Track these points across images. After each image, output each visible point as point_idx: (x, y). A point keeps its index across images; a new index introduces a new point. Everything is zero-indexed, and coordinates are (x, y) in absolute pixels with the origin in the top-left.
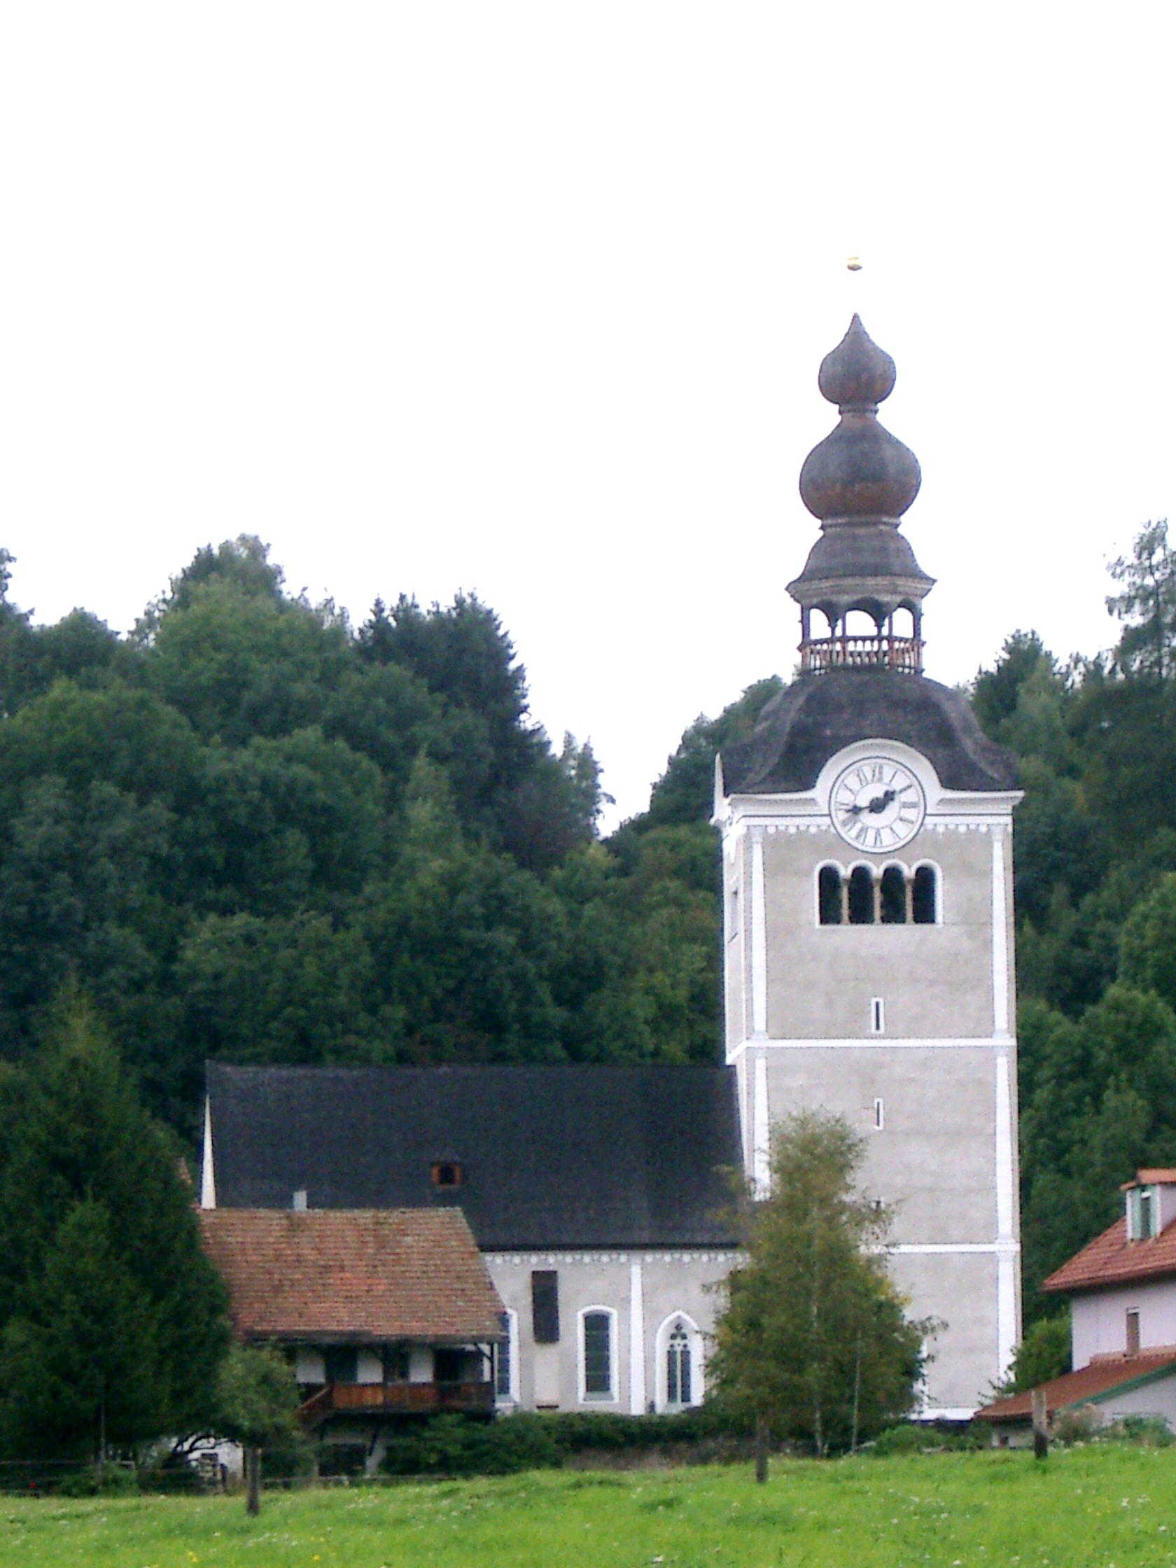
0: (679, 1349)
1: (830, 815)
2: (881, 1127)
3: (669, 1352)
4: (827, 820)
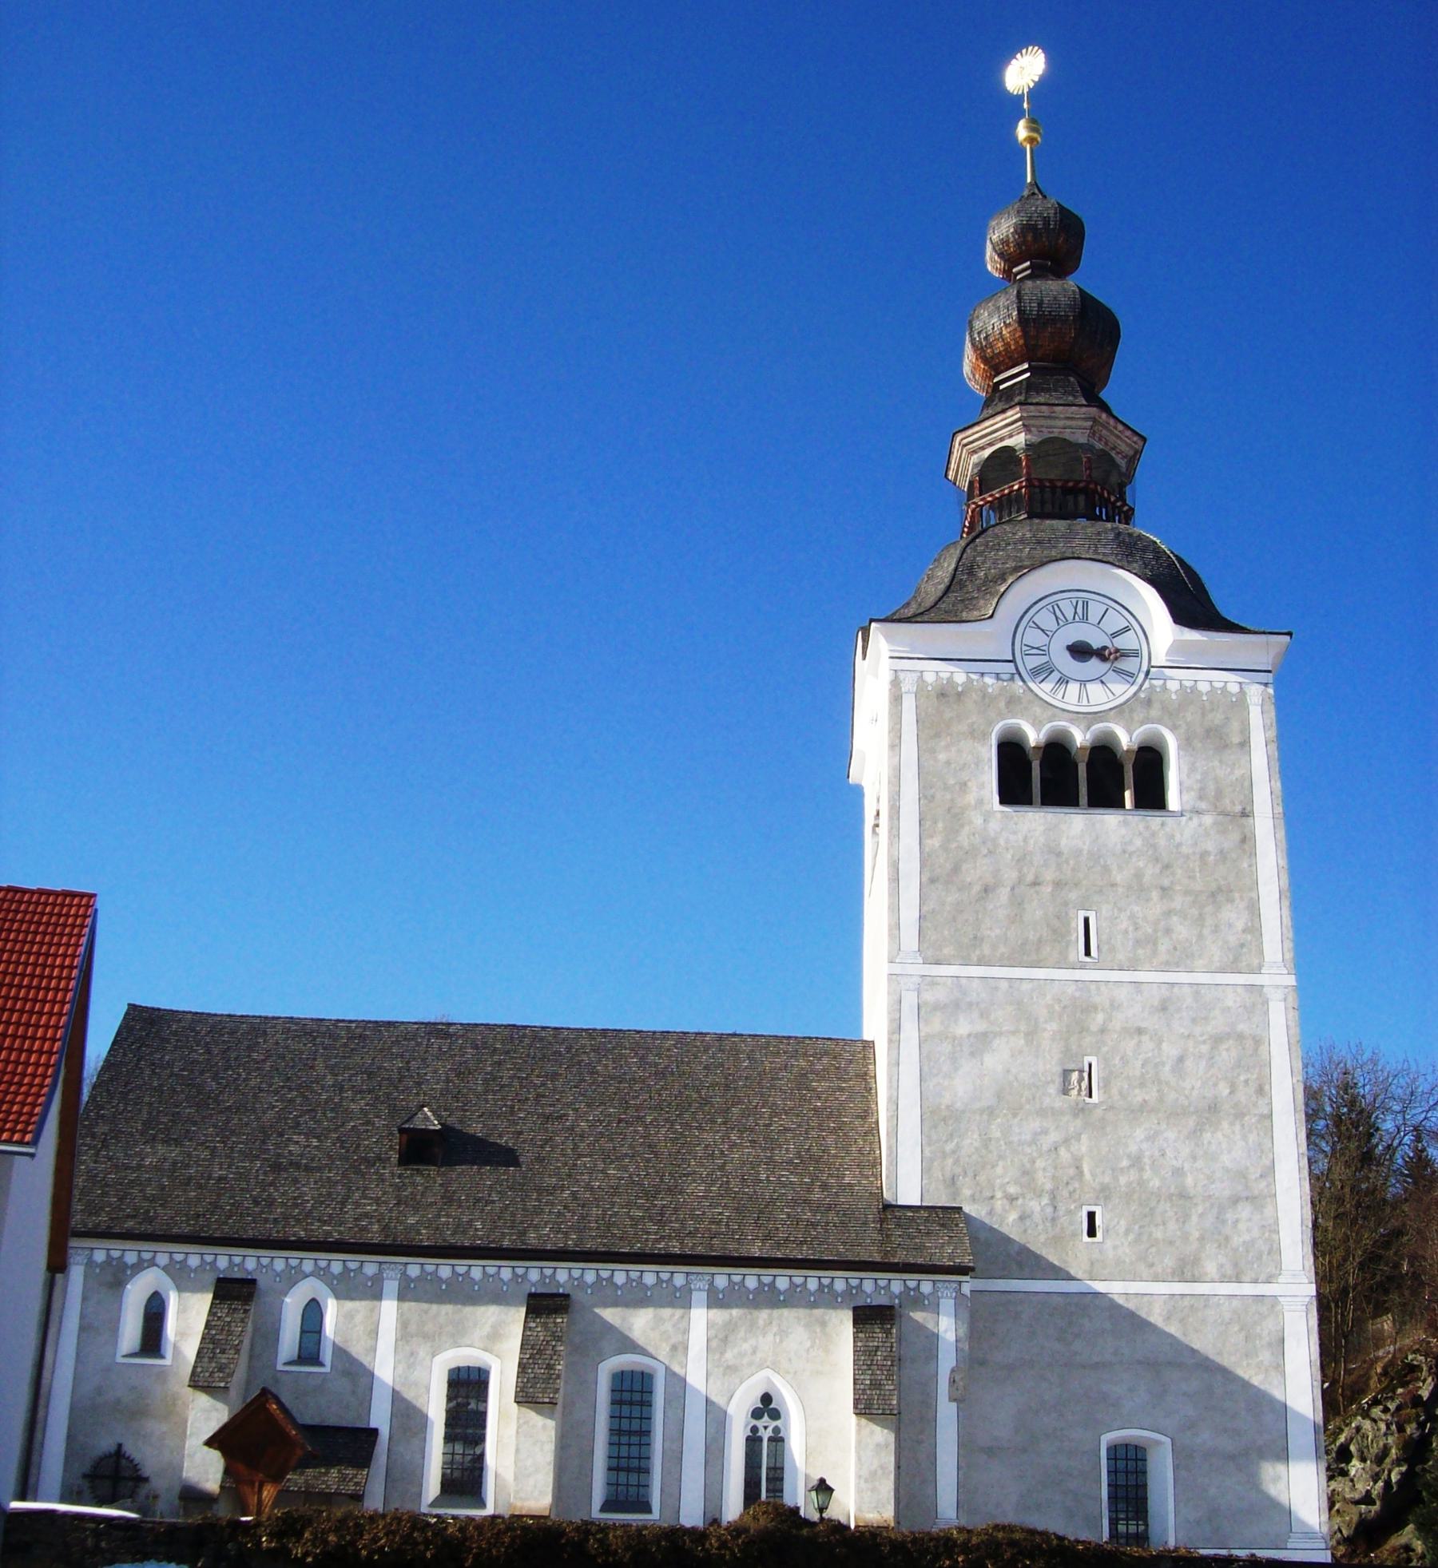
0: (766, 1435)
1: (1013, 661)
2: (1087, 1060)
3: (748, 1439)
4: (1010, 667)
